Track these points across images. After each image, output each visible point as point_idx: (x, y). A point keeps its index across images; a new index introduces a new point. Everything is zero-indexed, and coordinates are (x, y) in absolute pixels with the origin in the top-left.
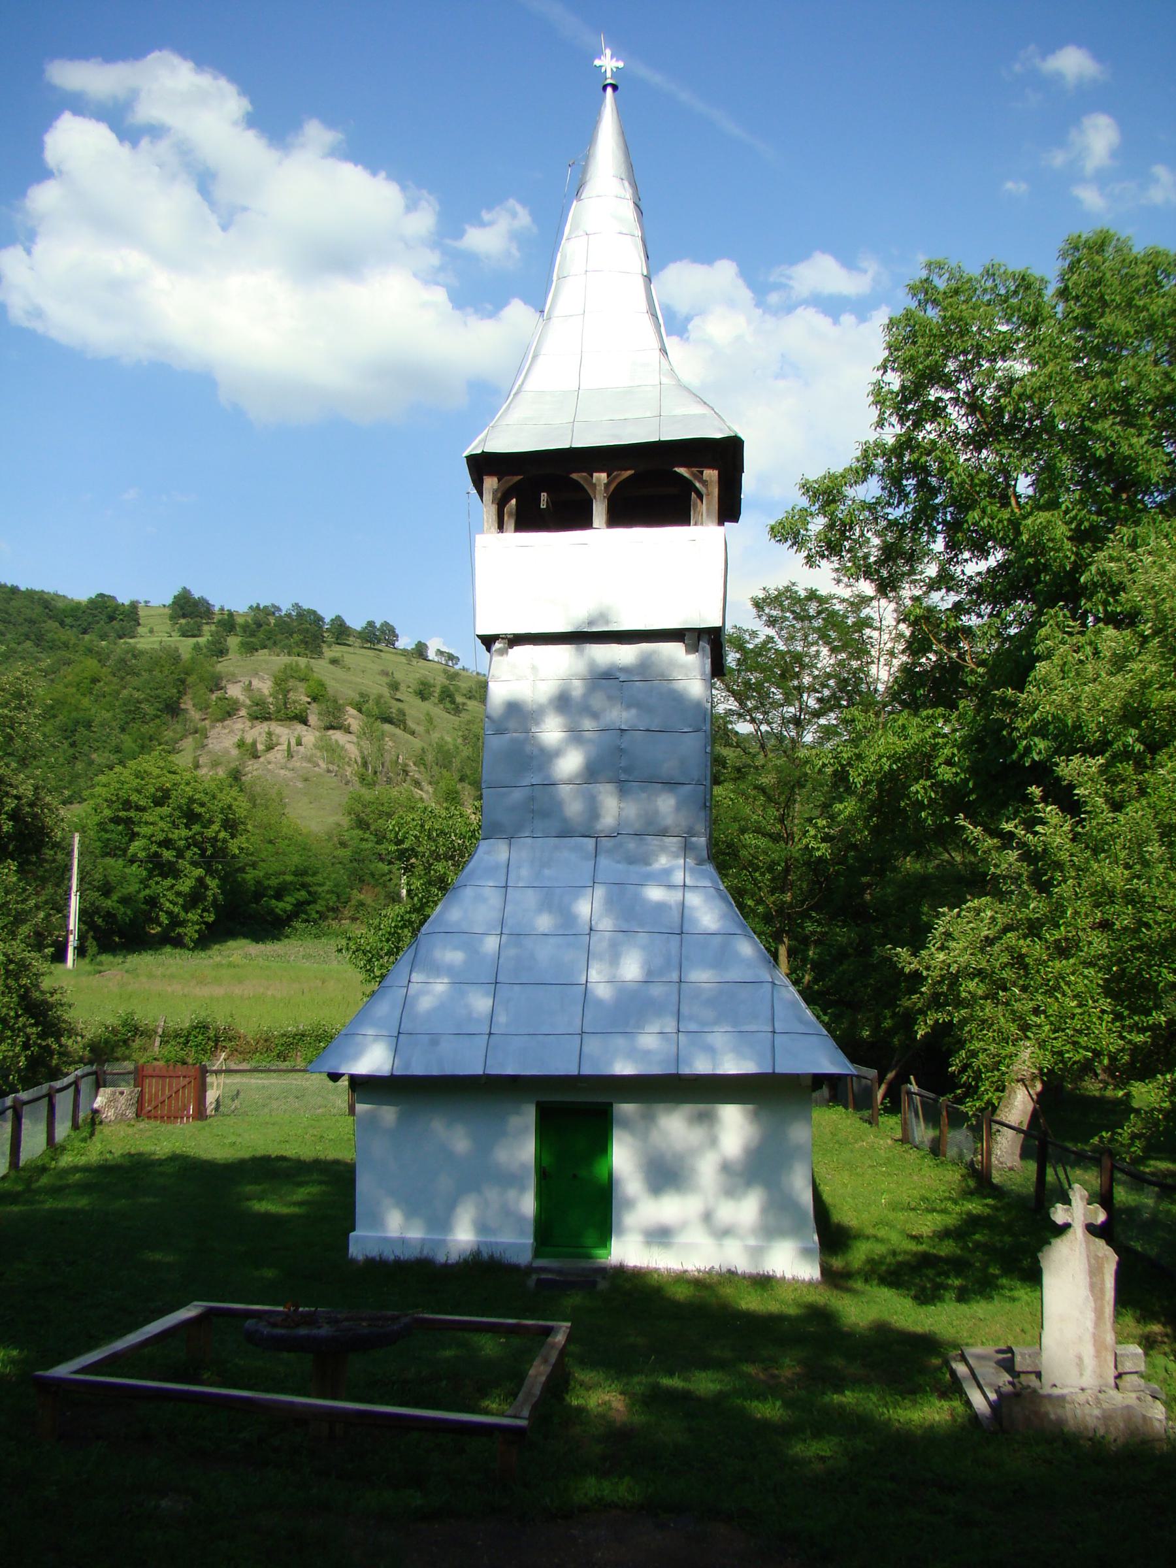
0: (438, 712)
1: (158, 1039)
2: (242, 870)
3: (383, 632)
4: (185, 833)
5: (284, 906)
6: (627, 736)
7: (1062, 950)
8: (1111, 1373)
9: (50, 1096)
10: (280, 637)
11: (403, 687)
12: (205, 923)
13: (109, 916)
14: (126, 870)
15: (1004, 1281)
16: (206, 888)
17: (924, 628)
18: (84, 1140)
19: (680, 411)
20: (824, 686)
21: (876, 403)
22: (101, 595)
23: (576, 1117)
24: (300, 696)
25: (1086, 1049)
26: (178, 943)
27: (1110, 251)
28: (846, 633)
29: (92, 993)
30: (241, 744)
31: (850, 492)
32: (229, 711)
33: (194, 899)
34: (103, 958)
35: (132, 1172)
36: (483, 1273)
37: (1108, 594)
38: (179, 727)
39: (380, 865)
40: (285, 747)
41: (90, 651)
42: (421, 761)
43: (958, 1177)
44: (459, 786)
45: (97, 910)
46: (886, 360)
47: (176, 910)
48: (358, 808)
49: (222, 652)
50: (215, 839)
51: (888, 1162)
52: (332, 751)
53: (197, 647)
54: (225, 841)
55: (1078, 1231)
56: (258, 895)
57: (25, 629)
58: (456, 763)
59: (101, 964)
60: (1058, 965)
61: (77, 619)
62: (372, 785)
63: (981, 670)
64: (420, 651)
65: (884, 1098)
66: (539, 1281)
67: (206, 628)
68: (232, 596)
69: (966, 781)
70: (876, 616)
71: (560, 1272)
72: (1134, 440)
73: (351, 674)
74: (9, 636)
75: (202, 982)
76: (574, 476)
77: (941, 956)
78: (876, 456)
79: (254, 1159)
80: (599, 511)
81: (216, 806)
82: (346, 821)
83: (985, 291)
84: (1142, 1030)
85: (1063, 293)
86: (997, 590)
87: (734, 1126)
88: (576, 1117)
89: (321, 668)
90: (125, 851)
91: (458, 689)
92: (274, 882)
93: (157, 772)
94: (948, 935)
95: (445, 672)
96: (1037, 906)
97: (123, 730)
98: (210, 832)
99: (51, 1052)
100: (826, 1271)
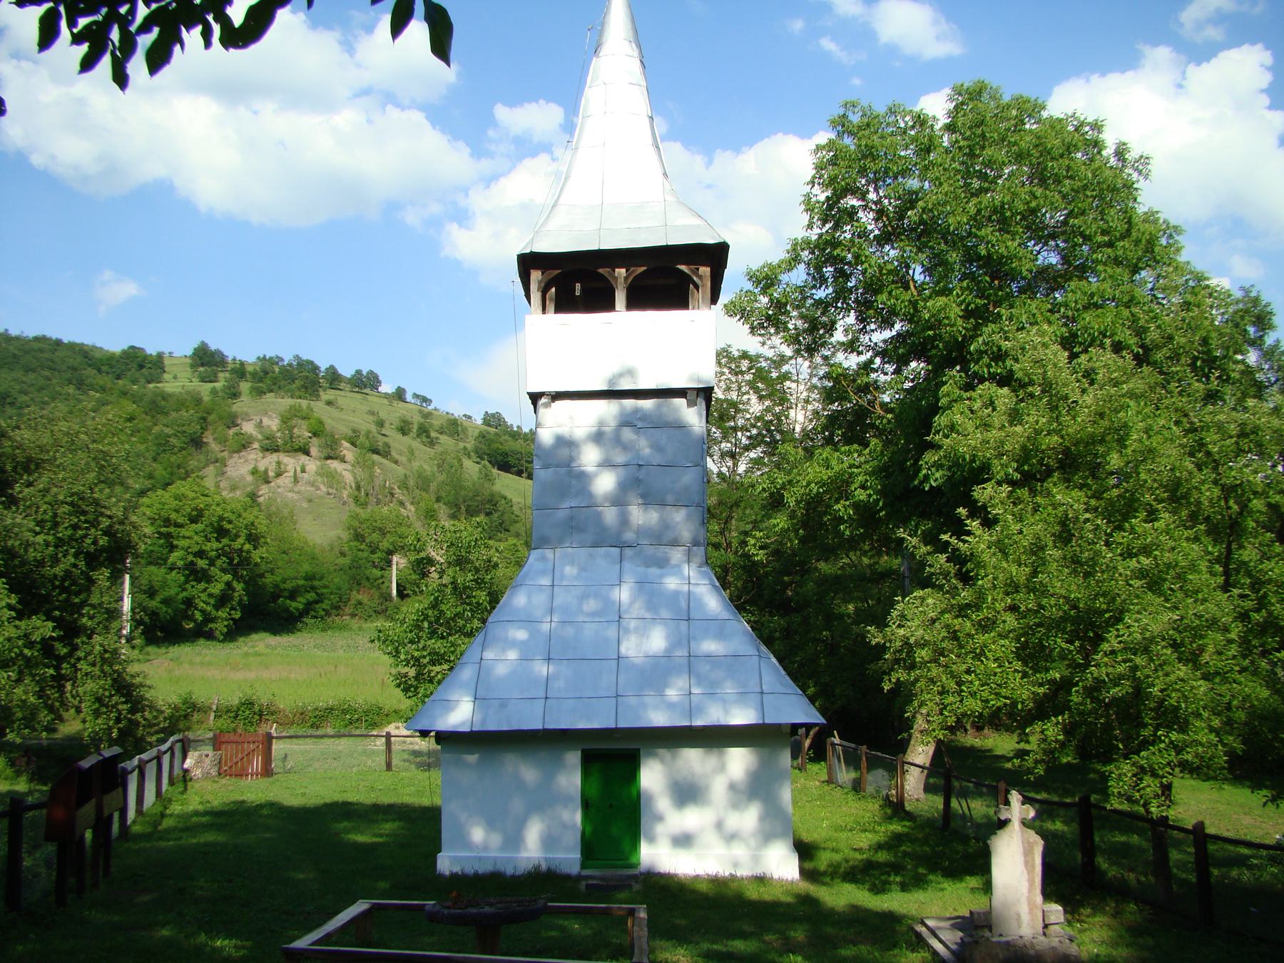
0: (416, 444)
1: (213, 714)
2: (262, 576)
3: (369, 379)
4: (216, 545)
5: (296, 605)
6: (644, 470)
7: (986, 626)
8: (1041, 925)
9: (158, 758)
10: (283, 383)
11: (387, 425)
12: (233, 619)
13: (154, 614)
14: (168, 577)
15: (931, 877)
16: (234, 590)
17: (836, 386)
18: (182, 793)
19: (680, 222)
20: (754, 426)
21: (807, 210)
22: (133, 347)
23: (611, 759)
24: (302, 432)
25: (1006, 698)
26: (210, 636)
27: (985, 96)
28: (769, 383)
29: (169, 675)
30: (254, 472)
31: (784, 278)
32: (244, 445)
33: (223, 600)
34: (150, 649)
35: (234, 817)
36: (544, 880)
37: (992, 360)
38: (202, 457)
39: (374, 571)
40: (292, 474)
41: (124, 393)
42: (404, 485)
43: (877, 806)
44: (436, 506)
45: (144, 609)
46: (814, 177)
47: (209, 608)
48: (356, 524)
49: (235, 395)
50: (241, 550)
51: (821, 797)
52: (332, 477)
53: (214, 392)
54: (248, 552)
55: (1016, 824)
56: (275, 597)
57: (68, 375)
58: (433, 486)
59: (148, 654)
60: (981, 638)
61: (111, 366)
62: (364, 505)
63: (890, 416)
64: (400, 394)
65: (809, 749)
66: (587, 886)
67: (221, 375)
68: (243, 347)
69: (877, 501)
70: (794, 371)
71: (602, 879)
72: (1009, 243)
73: (345, 414)
74: (54, 381)
75: (235, 668)
76: (601, 271)
77: (901, 632)
78: (803, 250)
79: (326, 805)
80: (620, 298)
81: (241, 523)
82: (345, 536)
83: (888, 124)
84: (1041, 685)
85: (950, 128)
86: (897, 353)
87: (739, 760)
88: (611, 759)
89: (319, 408)
90: (166, 560)
91: (431, 425)
92: (289, 585)
93: (192, 495)
94: (903, 616)
95: (420, 412)
96: (966, 595)
97: (155, 460)
98: (237, 545)
99: (138, 724)
100: (802, 871)
